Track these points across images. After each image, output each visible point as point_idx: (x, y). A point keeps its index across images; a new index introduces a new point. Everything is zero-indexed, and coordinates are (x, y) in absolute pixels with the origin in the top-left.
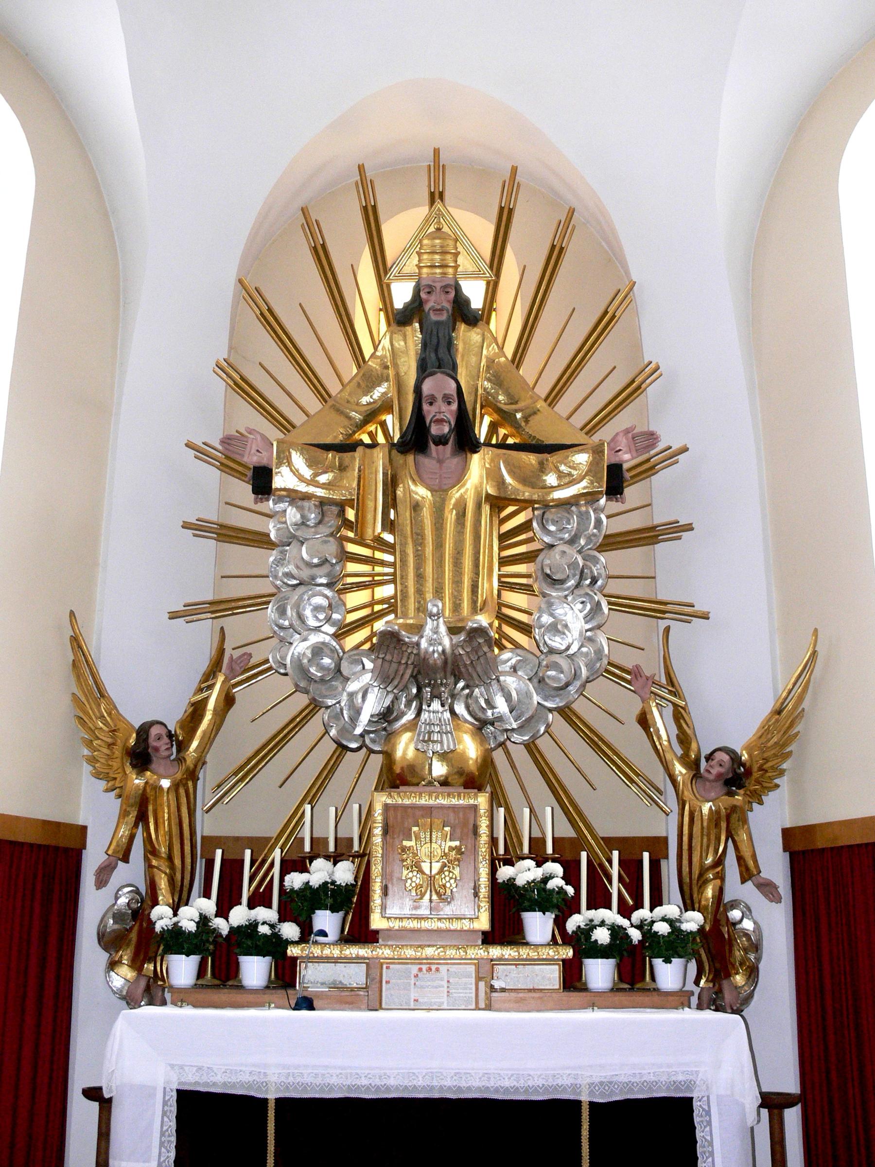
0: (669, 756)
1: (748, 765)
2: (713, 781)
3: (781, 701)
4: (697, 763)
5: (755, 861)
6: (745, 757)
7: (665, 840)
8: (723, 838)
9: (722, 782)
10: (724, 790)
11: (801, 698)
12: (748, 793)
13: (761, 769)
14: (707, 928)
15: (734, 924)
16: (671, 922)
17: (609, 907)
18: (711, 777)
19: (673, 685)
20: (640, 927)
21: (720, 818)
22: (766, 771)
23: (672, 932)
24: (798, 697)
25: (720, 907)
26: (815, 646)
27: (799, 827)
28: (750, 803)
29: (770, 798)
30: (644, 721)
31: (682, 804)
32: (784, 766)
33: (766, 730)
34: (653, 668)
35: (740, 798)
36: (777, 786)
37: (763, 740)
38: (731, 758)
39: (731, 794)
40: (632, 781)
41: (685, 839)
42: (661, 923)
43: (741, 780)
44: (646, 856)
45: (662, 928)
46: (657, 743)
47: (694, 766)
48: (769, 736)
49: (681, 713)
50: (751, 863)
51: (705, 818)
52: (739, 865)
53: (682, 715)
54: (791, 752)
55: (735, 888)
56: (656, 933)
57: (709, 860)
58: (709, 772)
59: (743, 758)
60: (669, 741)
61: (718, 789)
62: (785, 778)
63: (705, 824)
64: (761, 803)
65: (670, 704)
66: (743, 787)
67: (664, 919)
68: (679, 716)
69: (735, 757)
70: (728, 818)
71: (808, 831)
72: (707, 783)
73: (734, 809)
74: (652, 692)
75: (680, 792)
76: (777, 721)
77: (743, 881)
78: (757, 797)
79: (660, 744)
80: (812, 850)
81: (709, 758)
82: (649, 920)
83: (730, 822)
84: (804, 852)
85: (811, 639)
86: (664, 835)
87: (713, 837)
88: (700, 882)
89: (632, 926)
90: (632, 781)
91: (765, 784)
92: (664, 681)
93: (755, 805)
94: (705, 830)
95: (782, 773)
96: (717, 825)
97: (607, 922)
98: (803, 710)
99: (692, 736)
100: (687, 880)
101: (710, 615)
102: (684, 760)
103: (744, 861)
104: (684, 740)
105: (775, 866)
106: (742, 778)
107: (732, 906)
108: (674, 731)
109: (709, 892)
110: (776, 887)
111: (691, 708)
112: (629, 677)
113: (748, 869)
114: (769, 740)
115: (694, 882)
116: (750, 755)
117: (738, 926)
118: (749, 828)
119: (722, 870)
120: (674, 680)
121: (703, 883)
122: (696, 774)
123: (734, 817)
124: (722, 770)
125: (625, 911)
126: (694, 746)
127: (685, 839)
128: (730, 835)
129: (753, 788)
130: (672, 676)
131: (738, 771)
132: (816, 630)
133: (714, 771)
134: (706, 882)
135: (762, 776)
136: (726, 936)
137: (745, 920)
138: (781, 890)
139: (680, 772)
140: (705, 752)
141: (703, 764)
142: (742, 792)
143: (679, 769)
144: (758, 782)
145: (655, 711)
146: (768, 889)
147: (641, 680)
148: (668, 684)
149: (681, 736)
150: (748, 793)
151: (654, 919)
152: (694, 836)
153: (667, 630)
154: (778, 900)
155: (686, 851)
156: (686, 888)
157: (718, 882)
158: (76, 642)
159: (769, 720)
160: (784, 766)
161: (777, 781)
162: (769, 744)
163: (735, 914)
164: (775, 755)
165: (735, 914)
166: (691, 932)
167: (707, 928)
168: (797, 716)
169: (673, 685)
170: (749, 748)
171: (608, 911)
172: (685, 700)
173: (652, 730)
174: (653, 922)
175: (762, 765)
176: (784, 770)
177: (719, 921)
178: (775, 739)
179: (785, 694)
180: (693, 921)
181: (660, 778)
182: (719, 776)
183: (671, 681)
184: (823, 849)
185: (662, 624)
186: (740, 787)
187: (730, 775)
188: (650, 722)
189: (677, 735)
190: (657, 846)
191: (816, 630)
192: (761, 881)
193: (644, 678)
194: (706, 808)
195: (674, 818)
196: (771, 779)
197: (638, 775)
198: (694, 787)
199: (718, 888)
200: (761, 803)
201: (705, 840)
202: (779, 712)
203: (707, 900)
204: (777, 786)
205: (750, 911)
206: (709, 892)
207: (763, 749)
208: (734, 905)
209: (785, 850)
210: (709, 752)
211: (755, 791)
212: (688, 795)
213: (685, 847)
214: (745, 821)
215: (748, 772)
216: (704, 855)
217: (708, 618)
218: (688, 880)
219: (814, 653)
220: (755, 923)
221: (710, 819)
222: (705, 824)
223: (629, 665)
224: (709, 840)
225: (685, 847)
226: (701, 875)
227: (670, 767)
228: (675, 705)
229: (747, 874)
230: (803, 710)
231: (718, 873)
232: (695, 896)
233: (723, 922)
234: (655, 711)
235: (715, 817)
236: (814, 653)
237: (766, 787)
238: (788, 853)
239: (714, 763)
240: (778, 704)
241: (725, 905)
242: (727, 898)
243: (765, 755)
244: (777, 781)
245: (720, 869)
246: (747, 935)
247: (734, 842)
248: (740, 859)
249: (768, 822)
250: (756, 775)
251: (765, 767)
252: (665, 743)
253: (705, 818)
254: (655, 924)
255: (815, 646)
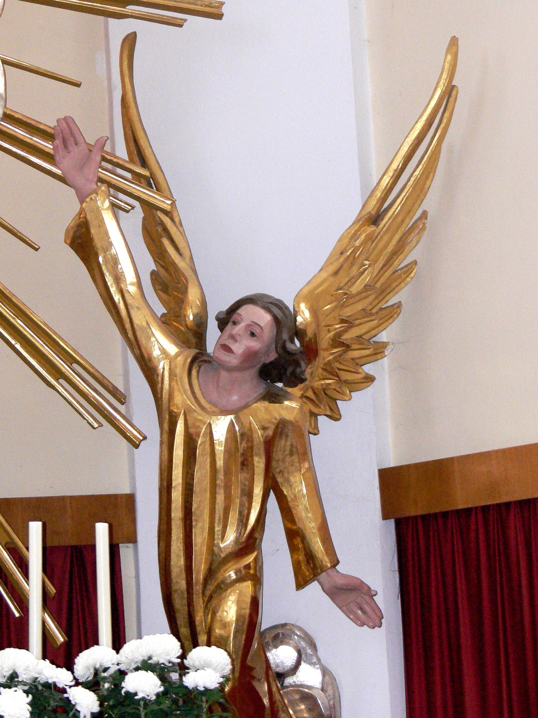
0: (140, 318)
1: (310, 333)
2: (239, 369)
3: (378, 194)
4: (198, 333)
5: (327, 540)
6: (304, 316)
7: (129, 501)
8: (258, 491)
9: (254, 371)
10: (261, 388)
11: (420, 189)
12: (310, 394)
13: (337, 342)
14: (227, 689)
15: (281, 676)
16: (160, 671)
17: (23, 643)
18: (232, 360)
19: (144, 163)
20: (93, 685)
21: (251, 448)
22: (348, 347)
23: (165, 693)
24: (415, 186)
25: (251, 640)
26: (451, 76)
27: (417, 466)
28: (314, 415)
29: (355, 406)
30: (83, 241)
31: (168, 420)
32: (383, 337)
33: (346, 259)
34: (101, 125)
35: (294, 404)
36: (369, 379)
37: (343, 279)
38: (276, 320)
39: (273, 397)
40: (59, 374)
41: (177, 495)
42: (142, 673)
43: (298, 364)
44: (102, 530)
45: (144, 685)
46: (113, 290)
47: (193, 340)
48: (354, 271)
49: (162, 224)
50: (318, 546)
51: (220, 449)
52: (293, 548)
53: (165, 229)
54: (399, 305)
55: (284, 599)
56: (130, 696)
57: (230, 539)
58: (226, 348)
59: (299, 319)
60: (139, 284)
61: (249, 385)
62: (385, 362)
63: (220, 463)
64: (335, 416)
65: (136, 203)
66: (303, 381)
67: (146, 665)
68: (158, 231)
69: (282, 316)
70: (269, 445)
71: (437, 471)
72: (224, 374)
73: (281, 427)
74: (101, 180)
75: (165, 395)
76: (370, 238)
77: (301, 583)
78: (326, 403)
79: (121, 292)
80: (445, 515)
81: (225, 320)
82: (113, 669)
83: (273, 457)
84: (426, 519)
85: (439, 58)
86: (127, 490)
87: (236, 492)
88: (211, 587)
89: (77, 683)
90: (59, 374)
91: (345, 376)
92: (121, 152)
93: (322, 420)
94: (221, 476)
95: (378, 351)
96: (246, 464)
97: (23, 676)
98: (425, 215)
99: (188, 273)
100: (179, 583)
101: (224, 10)
102: (171, 322)
103: (303, 539)
104: (170, 282)
105: (367, 550)
106: (295, 361)
107: (276, 637)
108: (148, 264)
109: (230, 610)
110: (370, 594)
111: (184, 212)
112: (47, 146)
113: (310, 557)
114: (352, 281)
115: (198, 588)
116: (314, 312)
117: (289, 681)
118: (311, 469)
119: (256, 560)
120: (147, 152)
121: (216, 590)
122: (200, 359)
123: (282, 446)
124: (255, 344)
125: (62, 655)
126: (193, 295)
127: (177, 495)
128: (272, 485)
129: (318, 384)
130: (143, 142)
131: (289, 346)
132: (454, 41)
133: (238, 348)
134: (223, 587)
135: (338, 358)
136: (266, 701)
137: (304, 666)
138: (379, 600)
139: (163, 351)
140: (218, 306)
141: (213, 334)
142: (296, 391)
143: (163, 346)
144: (330, 371)
145: (108, 217)
146: (352, 597)
147: (76, 152)
148: (131, 161)
149: (163, 273)
150: (310, 394)
151: (123, 667)
152: (196, 488)
153: (130, 42)
154: (374, 619)
155: (178, 521)
156: (180, 603)
157: (247, 587)
158: (126, 105)
159: (354, 236)
160: (383, 337)
161: (368, 369)
162: (356, 288)
163: (282, 656)
164: (366, 313)
165: (282, 656)
166: (207, 691)
167: (227, 689)
168: (414, 228)
169: (144, 163)
170: (313, 299)
171: (24, 651)
172: (170, 197)
173: (101, 259)
174: (122, 674)
175: (339, 335)
176: (385, 345)
177: (251, 669)
178: (366, 278)
179: (386, 180)
180: (209, 668)
181: (116, 363)
182: (250, 356)
183: (138, 152)
184: (468, 511)
185: (119, 29)
186: (296, 380)
187: (273, 356)
188: (98, 243)
189: (153, 274)
190: (118, 510)
191: (454, 41)
192: (340, 581)
193: (83, 147)
194: (221, 427)
195: (150, 455)
196: (358, 363)
197: (70, 359)
198: (195, 381)
199: (248, 600)
200: (335, 416)
201: (220, 498)
202: (375, 219)
203: (225, 625)
204: (369, 379)
205: (313, 646)
206: (230, 610)
207: (344, 299)
208: (280, 635)
209: (386, 516)
210: (225, 307)
211: (325, 389)
212: (181, 399)
213: (177, 513)
214: (304, 453)
215: (311, 351)
216: (218, 528)
217: (220, 17)
218: (183, 584)
219: (450, 92)
220: (325, 672)
221: (229, 452)
222: (220, 463)
223: (48, 120)
224: (228, 498)
225: (177, 513)
226: (211, 573)
227: (143, 340)
228: (146, 205)
229: (308, 568)
230: (425, 215)
231: (248, 567)
232: (199, 617)
233: (259, 672)
234: (108, 217)
235: (241, 448)
236: (450, 92)
237: (346, 382)
238: (391, 524)
239: (238, 329)
240: (373, 202)
241: (262, 634)
242: (266, 621)
243: (347, 312)
244: (368, 369)
245: (250, 559)
246: (307, 698)
247: (281, 499)
248: (294, 535)
249: (352, 455)
250: (326, 355)
251: (346, 337)
252: (132, 289)
253: (220, 449)
254: (128, 678)
255: (451, 76)
